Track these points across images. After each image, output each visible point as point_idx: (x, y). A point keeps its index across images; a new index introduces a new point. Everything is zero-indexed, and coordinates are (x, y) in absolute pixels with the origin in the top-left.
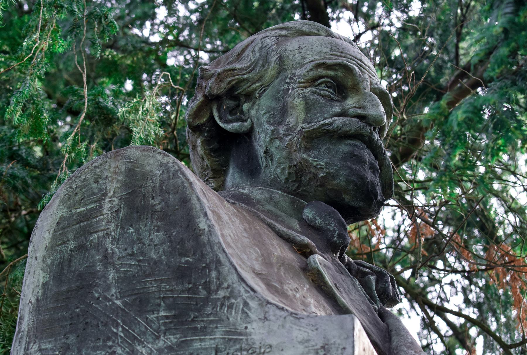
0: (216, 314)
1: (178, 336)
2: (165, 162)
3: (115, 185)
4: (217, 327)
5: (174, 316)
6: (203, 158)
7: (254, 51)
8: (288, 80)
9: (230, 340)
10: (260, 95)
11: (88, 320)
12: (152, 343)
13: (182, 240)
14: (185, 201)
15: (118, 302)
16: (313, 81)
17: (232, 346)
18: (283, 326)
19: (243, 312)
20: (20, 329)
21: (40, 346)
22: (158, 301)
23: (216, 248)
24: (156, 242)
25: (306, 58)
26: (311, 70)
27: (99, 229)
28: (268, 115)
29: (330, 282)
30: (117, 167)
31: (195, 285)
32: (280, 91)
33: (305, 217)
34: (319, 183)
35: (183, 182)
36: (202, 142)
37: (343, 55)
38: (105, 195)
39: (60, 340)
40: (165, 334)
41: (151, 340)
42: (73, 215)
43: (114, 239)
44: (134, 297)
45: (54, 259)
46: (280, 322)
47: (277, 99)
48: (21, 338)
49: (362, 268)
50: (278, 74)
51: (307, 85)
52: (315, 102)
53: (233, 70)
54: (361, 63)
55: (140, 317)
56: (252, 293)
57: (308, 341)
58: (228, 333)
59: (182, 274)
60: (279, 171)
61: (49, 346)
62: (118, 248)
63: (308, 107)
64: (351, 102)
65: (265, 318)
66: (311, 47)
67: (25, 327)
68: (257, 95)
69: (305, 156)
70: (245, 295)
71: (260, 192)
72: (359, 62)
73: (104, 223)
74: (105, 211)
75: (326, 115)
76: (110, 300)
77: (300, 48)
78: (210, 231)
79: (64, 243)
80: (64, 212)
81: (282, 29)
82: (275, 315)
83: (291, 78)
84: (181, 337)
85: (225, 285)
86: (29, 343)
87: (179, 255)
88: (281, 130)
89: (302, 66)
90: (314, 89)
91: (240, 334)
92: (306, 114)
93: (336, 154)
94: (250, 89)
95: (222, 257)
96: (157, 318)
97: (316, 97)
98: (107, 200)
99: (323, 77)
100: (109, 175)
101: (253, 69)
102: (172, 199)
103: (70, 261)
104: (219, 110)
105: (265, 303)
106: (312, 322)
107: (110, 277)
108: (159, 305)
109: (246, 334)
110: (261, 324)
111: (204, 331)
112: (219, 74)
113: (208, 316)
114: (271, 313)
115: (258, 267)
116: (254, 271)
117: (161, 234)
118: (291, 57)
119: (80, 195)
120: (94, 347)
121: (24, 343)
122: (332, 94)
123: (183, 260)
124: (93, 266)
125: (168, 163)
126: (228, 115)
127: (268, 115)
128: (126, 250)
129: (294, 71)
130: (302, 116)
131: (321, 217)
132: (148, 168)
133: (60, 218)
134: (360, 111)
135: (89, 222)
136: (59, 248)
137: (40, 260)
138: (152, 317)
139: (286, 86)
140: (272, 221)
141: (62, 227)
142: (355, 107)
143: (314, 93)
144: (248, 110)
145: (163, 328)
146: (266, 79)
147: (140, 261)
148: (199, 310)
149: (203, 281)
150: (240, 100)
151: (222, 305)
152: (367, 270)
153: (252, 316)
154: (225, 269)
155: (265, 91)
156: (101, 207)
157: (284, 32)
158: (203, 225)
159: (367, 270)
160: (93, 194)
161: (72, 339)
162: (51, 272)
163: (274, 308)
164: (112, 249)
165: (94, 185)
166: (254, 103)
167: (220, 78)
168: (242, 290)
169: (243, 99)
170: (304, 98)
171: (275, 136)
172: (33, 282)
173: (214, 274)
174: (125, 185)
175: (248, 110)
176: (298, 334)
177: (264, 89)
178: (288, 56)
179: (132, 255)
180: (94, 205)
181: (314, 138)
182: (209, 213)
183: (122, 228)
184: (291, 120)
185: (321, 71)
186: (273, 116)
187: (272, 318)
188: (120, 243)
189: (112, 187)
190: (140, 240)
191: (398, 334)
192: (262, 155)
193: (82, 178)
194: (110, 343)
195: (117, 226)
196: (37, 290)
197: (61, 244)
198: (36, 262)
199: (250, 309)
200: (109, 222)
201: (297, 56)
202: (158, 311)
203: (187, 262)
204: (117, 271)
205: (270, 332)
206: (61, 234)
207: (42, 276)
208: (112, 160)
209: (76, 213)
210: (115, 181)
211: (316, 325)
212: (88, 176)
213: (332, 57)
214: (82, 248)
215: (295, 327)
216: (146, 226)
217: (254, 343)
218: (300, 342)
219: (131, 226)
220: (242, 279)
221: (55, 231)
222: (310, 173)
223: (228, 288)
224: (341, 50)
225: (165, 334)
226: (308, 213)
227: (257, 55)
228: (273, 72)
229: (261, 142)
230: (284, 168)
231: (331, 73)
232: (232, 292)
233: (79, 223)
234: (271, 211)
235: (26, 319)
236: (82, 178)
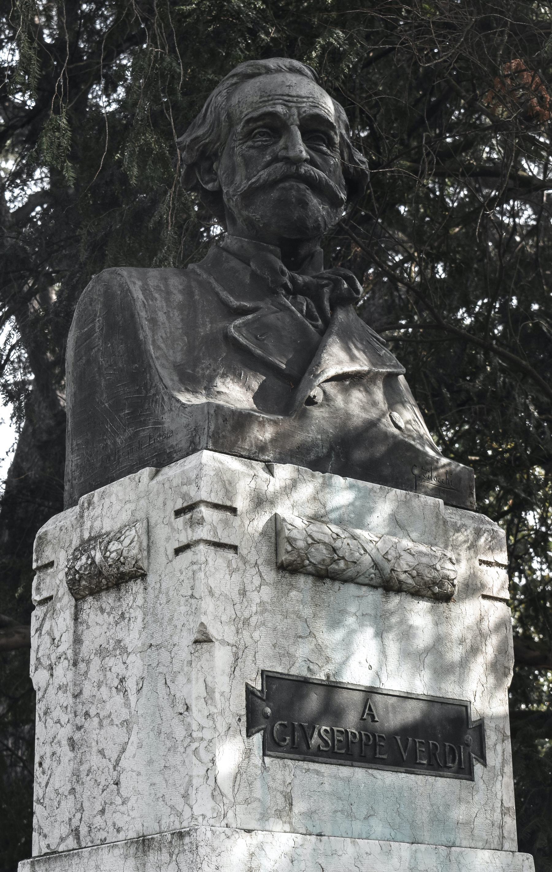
50: (229, 131)
51: (245, 140)
53: (197, 138)
63: (248, 162)
72: (286, 98)
81: (233, 76)
92: (246, 170)
95: (152, 364)
97: (252, 151)
99: (255, 129)
122: (266, 141)
155: (224, 149)
157: (235, 80)
158: (141, 337)
165: (90, 308)
214: (88, 362)
224: (269, 93)
231: (260, 123)
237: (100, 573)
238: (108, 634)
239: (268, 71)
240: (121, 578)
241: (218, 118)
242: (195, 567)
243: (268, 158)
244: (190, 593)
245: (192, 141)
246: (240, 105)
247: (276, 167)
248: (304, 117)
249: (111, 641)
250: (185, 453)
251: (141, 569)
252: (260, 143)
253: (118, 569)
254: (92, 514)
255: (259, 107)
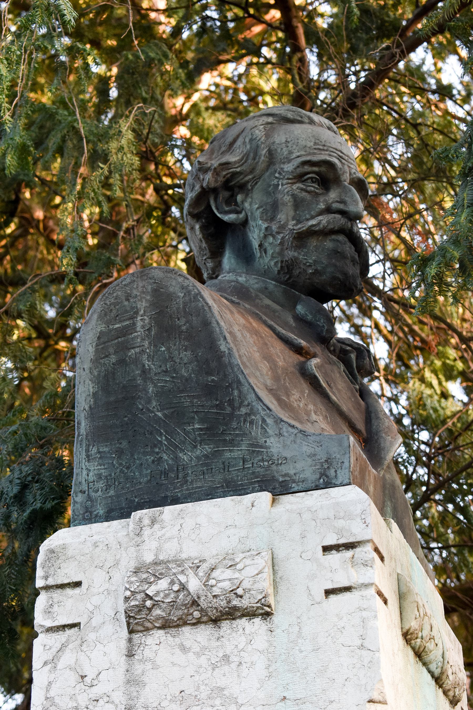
0: (240, 429)
1: (212, 446)
2: (186, 284)
3: (144, 304)
4: (242, 440)
5: (207, 429)
6: (201, 241)
7: (244, 143)
8: (277, 175)
9: (254, 451)
10: (253, 187)
11: (136, 429)
12: (191, 451)
13: (207, 360)
14: (206, 324)
15: (159, 414)
16: (300, 177)
17: (255, 457)
18: (295, 442)
19: (262, 428)
20: (79, 433)
21: (98, 449)
22: (193, 414)
23: (236, 369)
24: (185, 361)
25: (292, 153)
26: (298, 167)
27: (135, 345)
28: (261, 210)
29: (324, 385)
30: (144, 287)
31: (221, 402)
32: (270, 186)
33: (297, 312)
34: (307, 277)
35: (203, 306)
36: (200, 228)
37: (325, 148)
38: (137, 313)
39: (115, 444)
40: (201, 443)
41: (190, 449)
42: (110, 331)
43: (149, 356)
44: (172, 410)
45: (100, 371)
46: (292, 438)
47: (268, 194)
48: (81, 441)
49: (344, 346)
52: (303, 200)
53: (227, 163)
54: (341, 154)
55: (179, 428)
56: (268, 411)
57: (315, 455)
58: (252, 445)
59: (210, 391)
60: (272, 263)
61: (106, 449)
62: (154, 365)
63: (298, 204)
64: (333, 195)
65: (280, 434)
66: (296, 141)
67: (83, 431)
68: (250, 188)
69: (296, 254)
70: (263, 413)
71: (256, 281)
72: (339, 153)
73: (139, 340)
74: (138, 329)
75: (312, 213)
76: (152, 412)
77: (287, 142)
78: (229, 353)
79: (107, 356)
80: (102, 327)
82: (287, 432)
83: (280, 173)
84: (214, 448)
85: (246, 403)
86: (89, 445)
87: (206, 373)
88: (274, 227)
89: (289, 161)
90: (301, 185)
91: (261, 447)
92: (295, 211)
93: (323, 250)
94: (243, 181)
95: (242, 380)
96: (193, 429)
97: (304, 194)
98: (139, 318)
100: (138, 294)
101: (246, 162)
102: (195, 321)
103: (114, 374)
104: (216, 200)
105: (279, 421)
106: (318, 439)
107: (150, 391)
108: (193, 418)
109: (266, 448)
110: (277, 439)
111: (232, 443)
112: (215, 169)
113: (234, 429)
114: (284, 429)
115: (269, 382)
116: (266, 387)
117: (189, 353)
118: (279, 150)
119: (115, 312)
120: (144, 452)
121: (84, 445)
122: (317, 188)
123: (210, 378)
124: (134, 380)
125: (188, 286)
126: (224, 206)
127: (261, 210)
128: (161, 367)
129: (282, 166)
130: (292, 213)
131: (311, 313)
132: (171, 289)
133: (100, 333)
134: (341, 206)
135: (126, 338)
136: (102, 361)
137: (87, 371)
138: (189, 428)
139: (275, 182)
140: (272, 323)
141: (102, 341)
142: (337, 202)
143: (302, 189)
144: (243, 202)
145: (199, 438)
146: (258, 172)
147: (173, 377)
148: (226, 425)
149: (228, 399)
150: (233, 190)
151: (245, 421)
152: (348, 348)
153: (270, 432)
154: (245, 388)
155: (256, 183)
156: (134, 324)
158: (223, 348)
159: (348, 348)
160: (126, 311)
161: (124, 444)
162: (98, 383)
163: (286, 425)
164: (148, 366)
165: (126, 303)
166: (247, 195)
167: (216, 172)
168: (260, 408)
169: (236, 190)
170: (293, 195)
171: (268, 232)
172: (85, 391)
173: (236, 393)
174: (153, 305)
175: (243, 202)
176: (306, 449)
177: (256, 180)
178: (276, 150)
179: (166, 371)
180: (128, 323)
181: (302, 238)
182: (228, 335)
183: (155, 346)
184: (281, 217)
185: (307, 168)
186: (265, 212)
187: (285, 434)
188: (155, 360)
189: (142, 305)
190: (171, 358)
191: (378, 418)
192: (257, 247)
193: (115, 295)
194: (157, 450)
195: (150, 343)
196: (89, 399)
197: (104, 358)
198: (84, 373)
199: (267, 425)
200: (143, 340)
201: (284, 149)
202: (193, 423)
203: (213, 381)
204: (155, 386)
205: (285, 446)
206: (102, 348)
207: (91, 386)
208: (139, 279)
209: (113, 329)
210: (144, 301)
211: (320, 442)
212: (119, 293)
213: (316, 151)
214: (122, 362)
215: (304, 443)
216: (175, 345)
217: (273, 456)
218: (308, 456)
219: (163, 344)
220: (259, 399)
221: (97, 345)
222: (300, 268)
223: (248, 406)
224: (323, 143)
225: (201, 443)
226: (300, 309)
227: (248, 147)
228: (263, 166)
229: (255, 236)
230: (277, 262)
231: (316, 169)
232: (252, 409)
233: (117, 338)
234: (269, 305)
235: (83, 424)
236: (115, 295)
237: (195, 603)
238: (197, 678)
239: (312, 122)
240: (228, 614)
241: (256, 151)
242: (365, 614)
243: (322, 206)
244: (359, 642)
245: (221, 165)
246: (289, 145)
247: (335, 218)
248: (353, 178)
249: (202, 687)
250: (313, 485)
251: (269, 606)
252: (313, 189)
253: (229, 602)
254: (159, 534)
255: (314, 154)
